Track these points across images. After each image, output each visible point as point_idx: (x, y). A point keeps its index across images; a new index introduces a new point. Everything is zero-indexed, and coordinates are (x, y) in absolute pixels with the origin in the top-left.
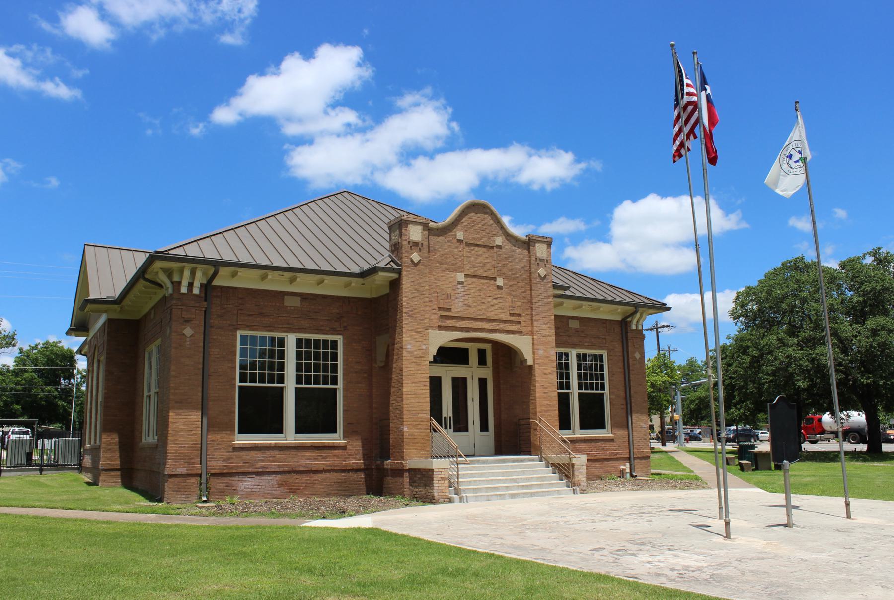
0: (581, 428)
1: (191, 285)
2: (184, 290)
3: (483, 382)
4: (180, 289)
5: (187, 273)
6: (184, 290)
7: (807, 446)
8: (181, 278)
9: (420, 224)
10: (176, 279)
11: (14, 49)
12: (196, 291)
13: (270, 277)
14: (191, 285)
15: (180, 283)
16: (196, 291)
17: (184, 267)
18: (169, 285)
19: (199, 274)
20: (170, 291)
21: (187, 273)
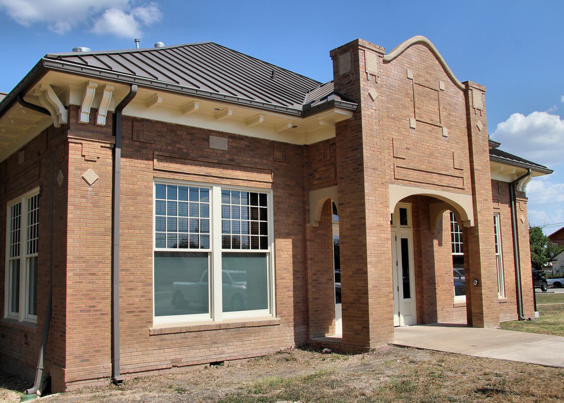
0: (224, 310)
1: (94, 112)
2: (84, 118)
3: (16, 308)
4: (77, 116)
5: (90, 93)
6: (84, 118)
7: (472, 224)
8: (82, 99)
9: (392, 60)
10: (73, 100)
11: (550, 109)
12: (101, 120)
13: (160, 100)
14: (94, 112)
15: (78, 108)
16: (101, 120)
17: (87, 84)
18: (63, 111)
19: (107, 96)
20: (64, 119)
21: (90, 93)
